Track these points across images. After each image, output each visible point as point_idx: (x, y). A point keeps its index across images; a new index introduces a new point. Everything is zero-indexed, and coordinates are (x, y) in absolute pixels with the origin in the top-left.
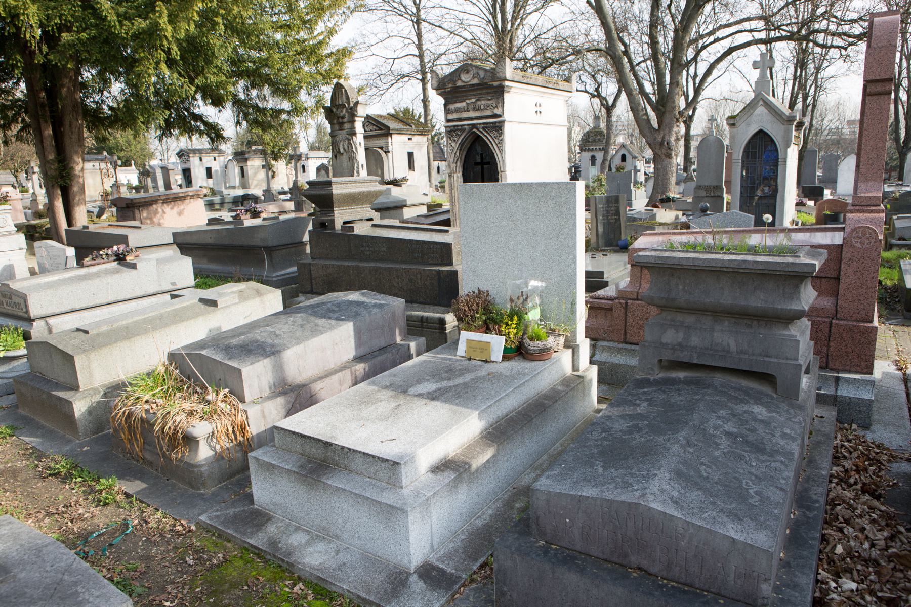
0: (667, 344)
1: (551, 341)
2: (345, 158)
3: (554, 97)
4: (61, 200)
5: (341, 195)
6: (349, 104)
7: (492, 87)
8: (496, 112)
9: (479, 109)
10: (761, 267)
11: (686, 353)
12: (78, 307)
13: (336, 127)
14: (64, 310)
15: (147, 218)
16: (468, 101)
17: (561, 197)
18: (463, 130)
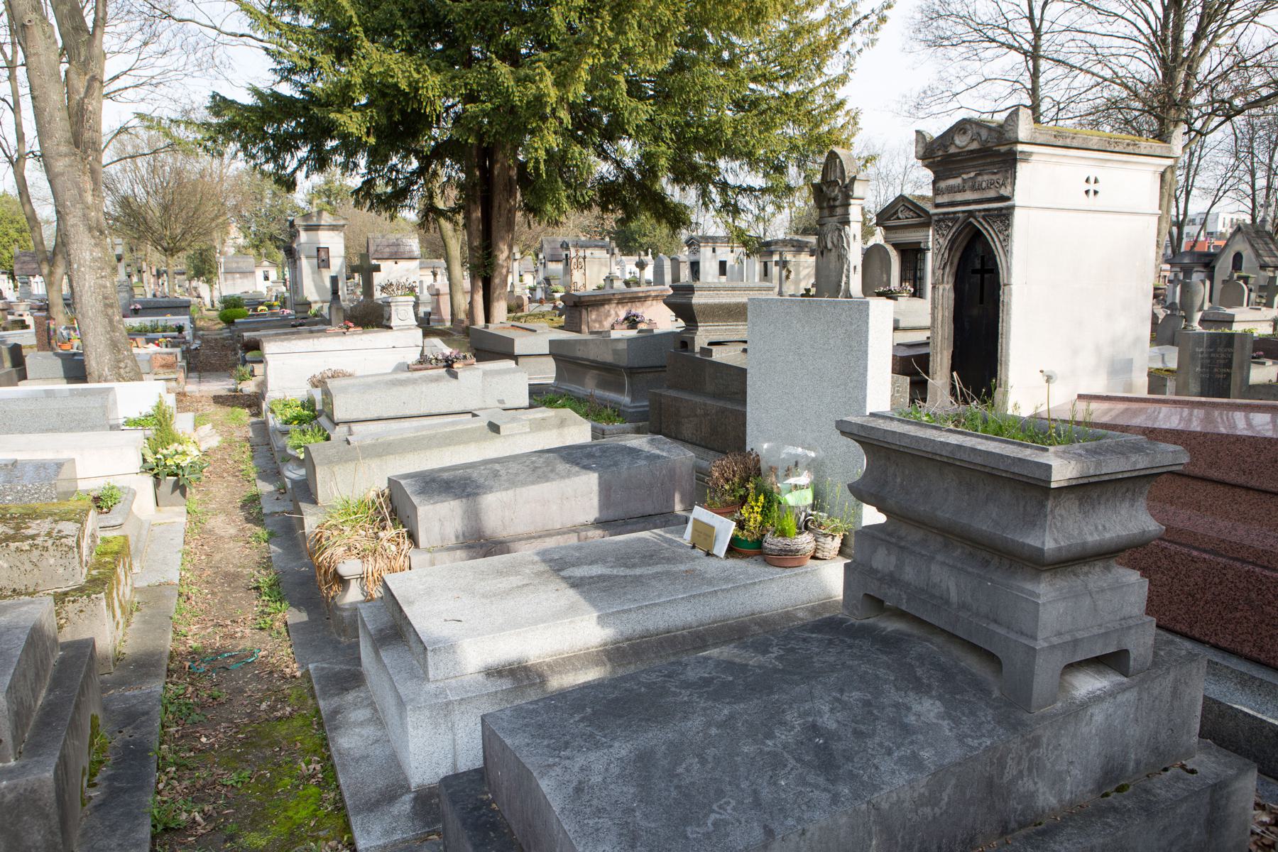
0: (877, 571)
1: (805, 541)
2: (833, 256)
3: (1109, 164)
4: (481, 292)
5: (706, 305)
6: (843, 180)
7: (998, 153)
8: (1005, 192)
9: (980, 189)
10: (979, 460)
11: (893, 590)
12: (385, 416)
13: (826, 212)
14: (369, 416)
15: (595, 321)
16: (965, 176)
17: (851, 324)
18: (955, 220)
